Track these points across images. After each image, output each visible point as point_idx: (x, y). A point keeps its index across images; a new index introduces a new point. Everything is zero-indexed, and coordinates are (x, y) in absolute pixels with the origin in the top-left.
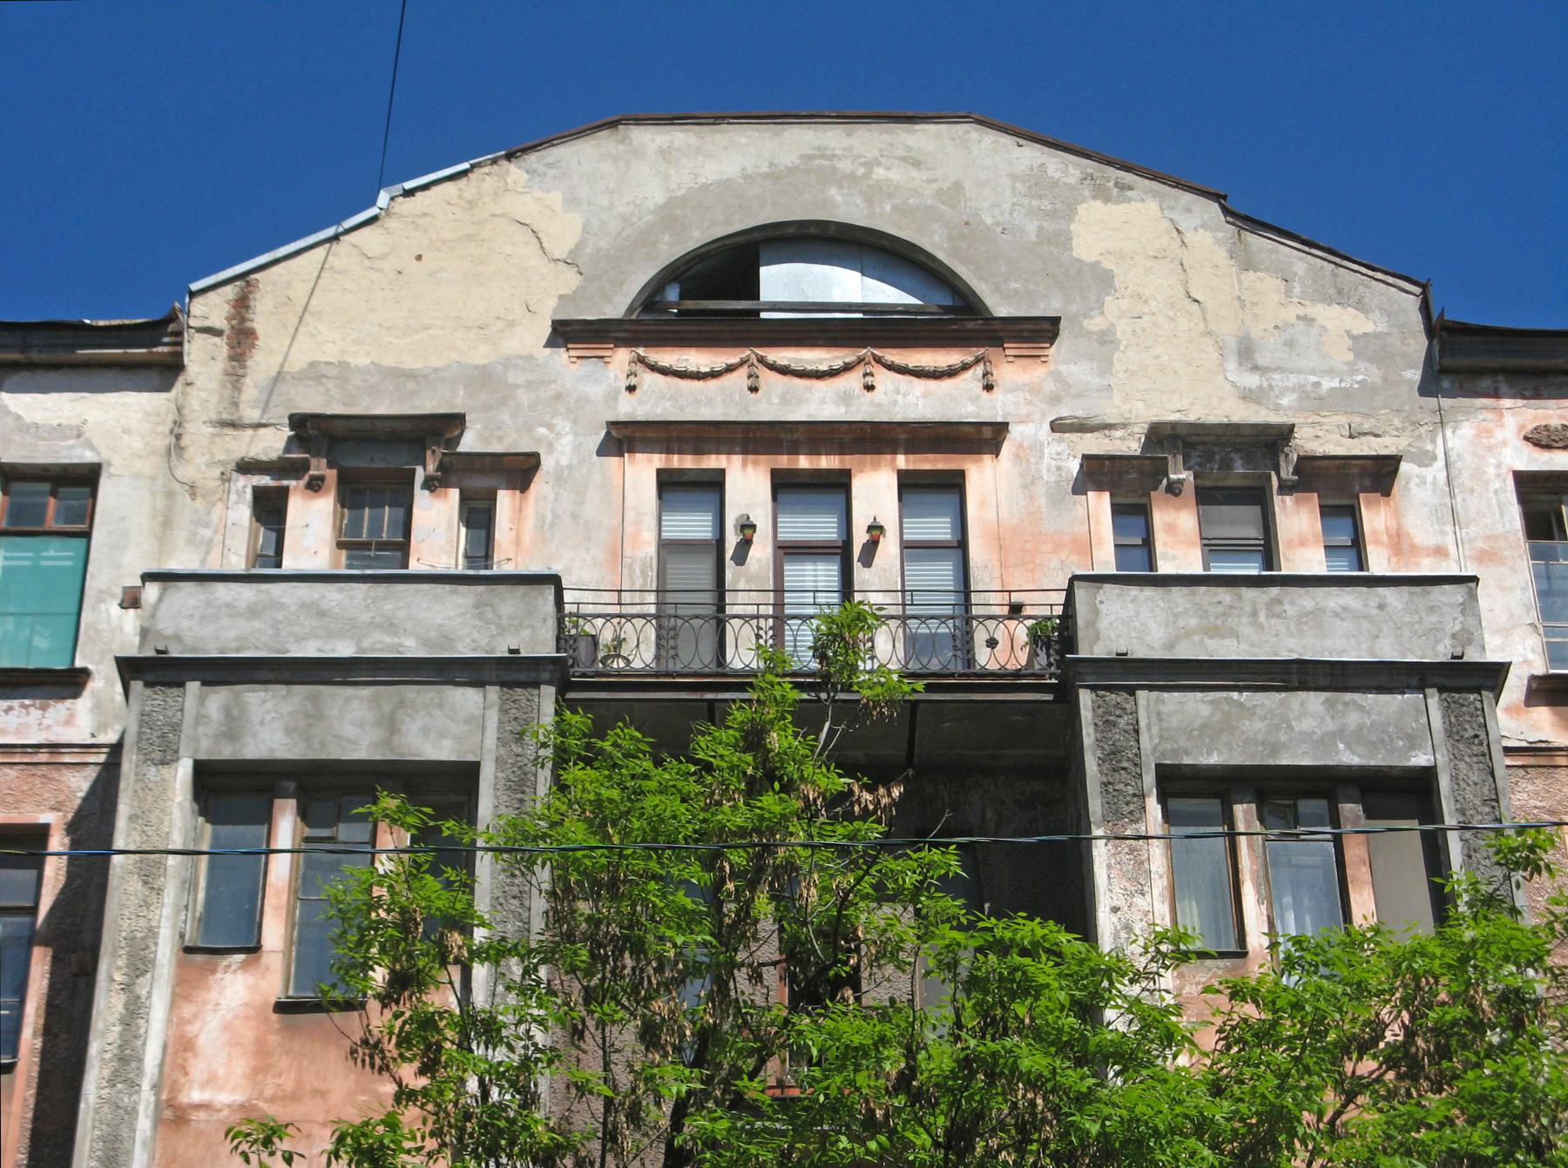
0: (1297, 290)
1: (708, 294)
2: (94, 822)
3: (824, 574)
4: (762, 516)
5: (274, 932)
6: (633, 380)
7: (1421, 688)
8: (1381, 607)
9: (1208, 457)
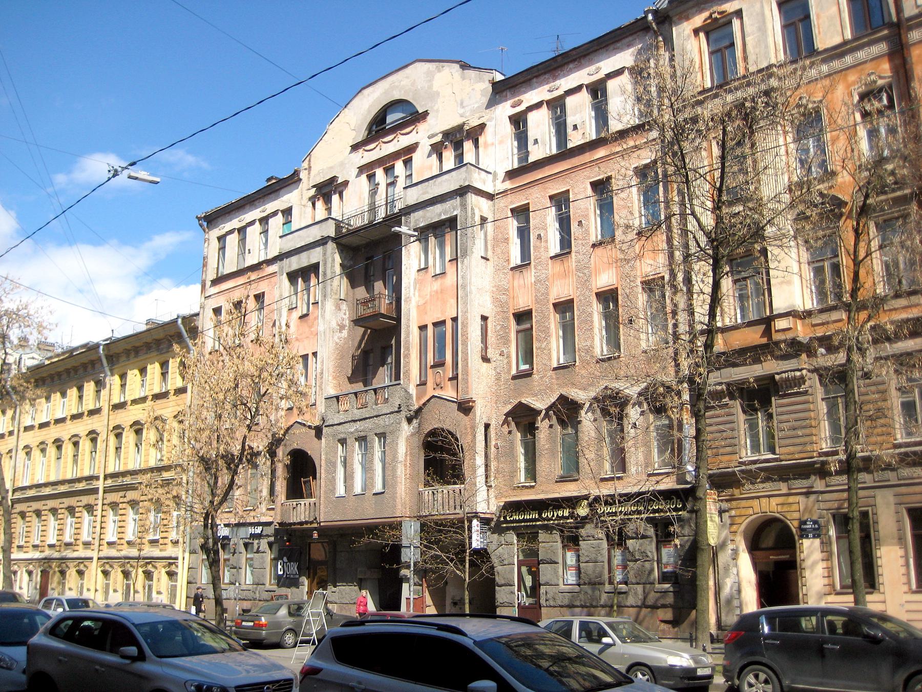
1: (378, 127)
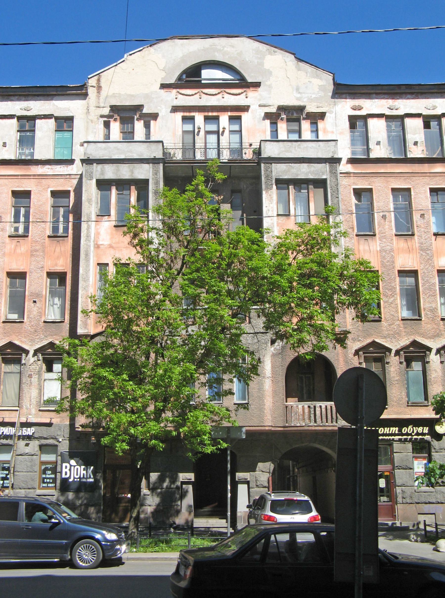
0: (308, 75)
1: (191, 77)
2: (79, 189)
3: (215, 137)
4: (202, 126)
5: (113, 212)
6: (177, 97)
7: (325, 163)
8: (319, 146)
9: (289, 112)
